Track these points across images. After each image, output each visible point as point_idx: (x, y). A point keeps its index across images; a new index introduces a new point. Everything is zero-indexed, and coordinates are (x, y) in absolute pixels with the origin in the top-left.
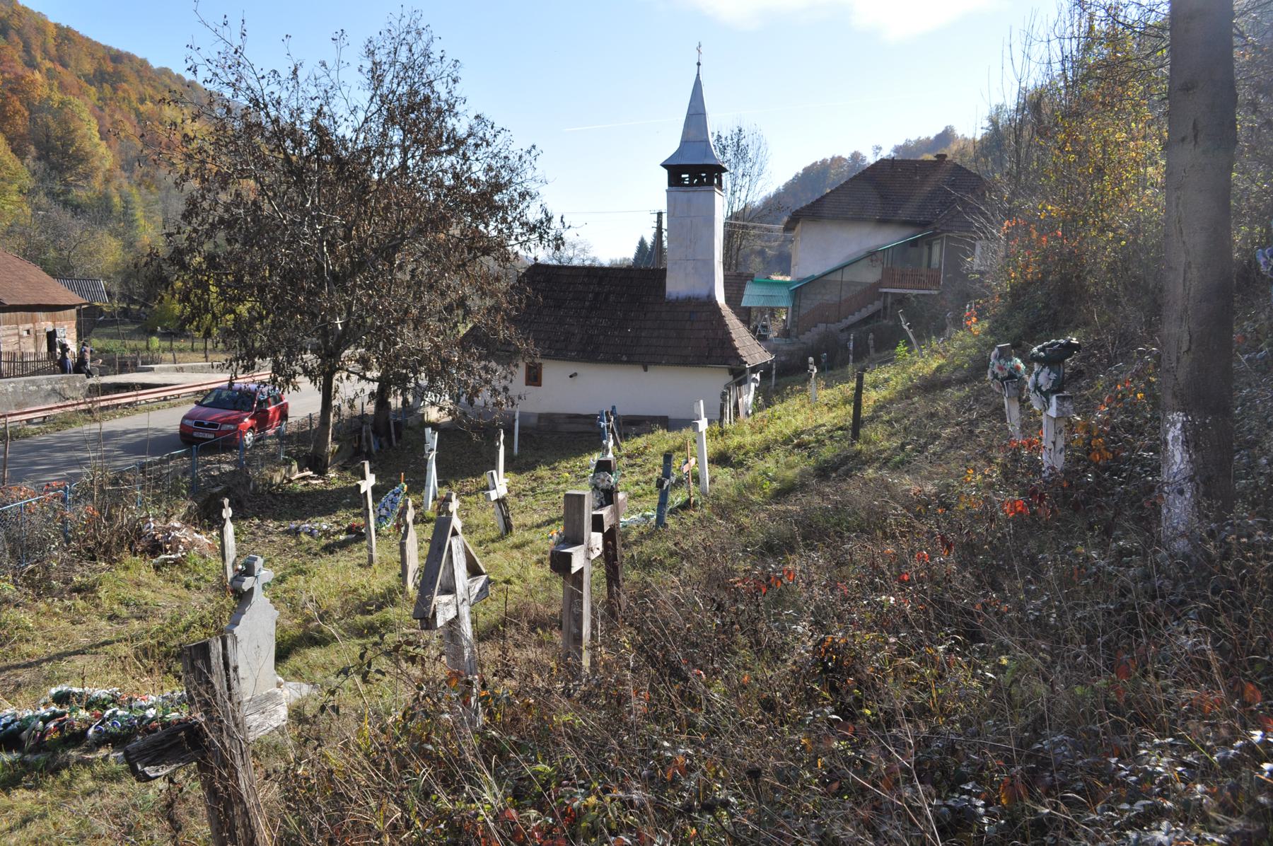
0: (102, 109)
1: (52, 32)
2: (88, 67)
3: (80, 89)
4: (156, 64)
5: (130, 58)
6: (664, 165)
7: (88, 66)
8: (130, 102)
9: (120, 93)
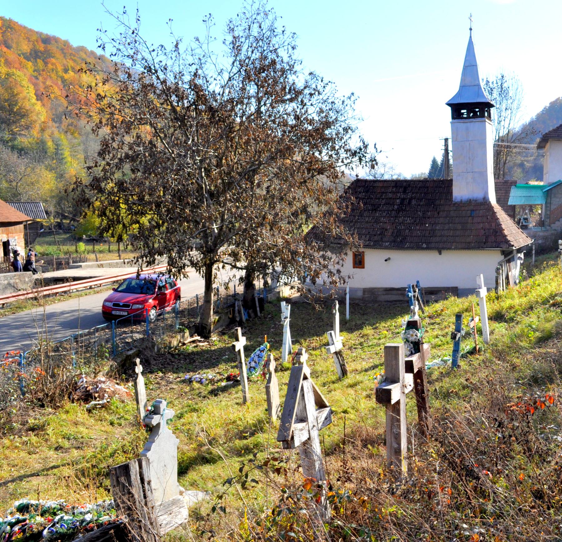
0: (37, 78)
5: (56, 40)
6: (449, 104)
8: (57, 72)
9: (50, 66)
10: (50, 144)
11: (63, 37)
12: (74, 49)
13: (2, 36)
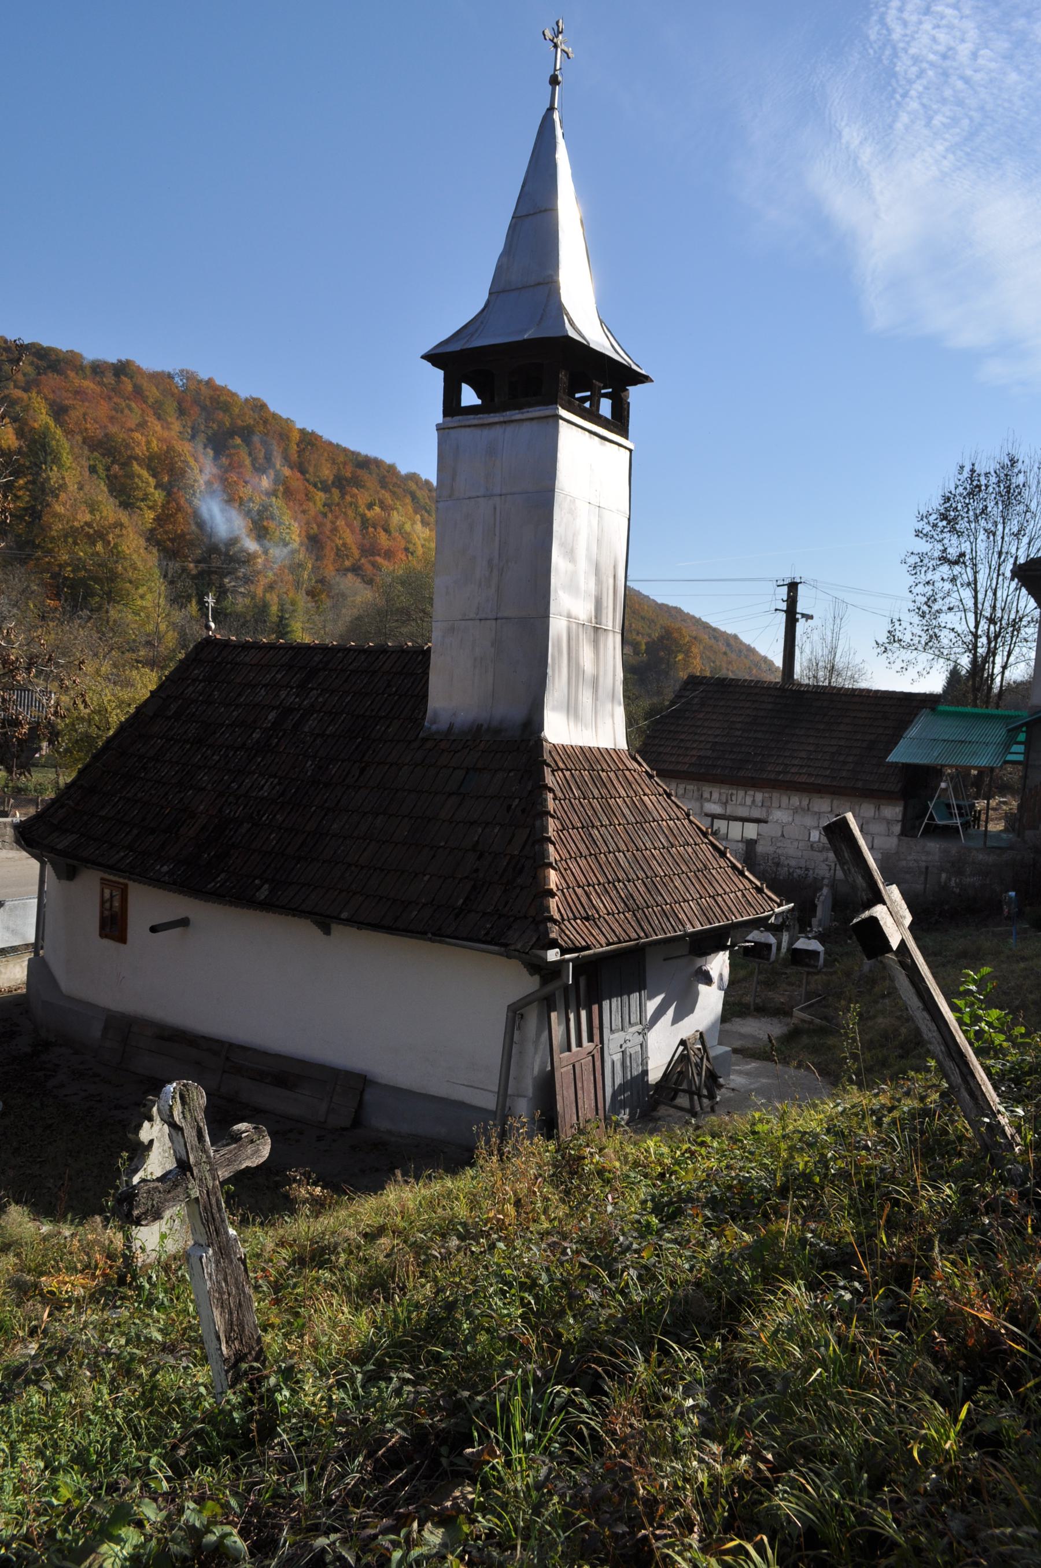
0: (325, 515)
1: (295, 437)
2: (327, 473)
3: (307, 495)
4: (403, 469)
5: (378, 463)
6: (434, 358)
7: (327, 472)
8: (356, 507)
9: (348, 498)
10: (274, 609)
11: (388, 460)
12: (401, 476)
13: (299, 457)
